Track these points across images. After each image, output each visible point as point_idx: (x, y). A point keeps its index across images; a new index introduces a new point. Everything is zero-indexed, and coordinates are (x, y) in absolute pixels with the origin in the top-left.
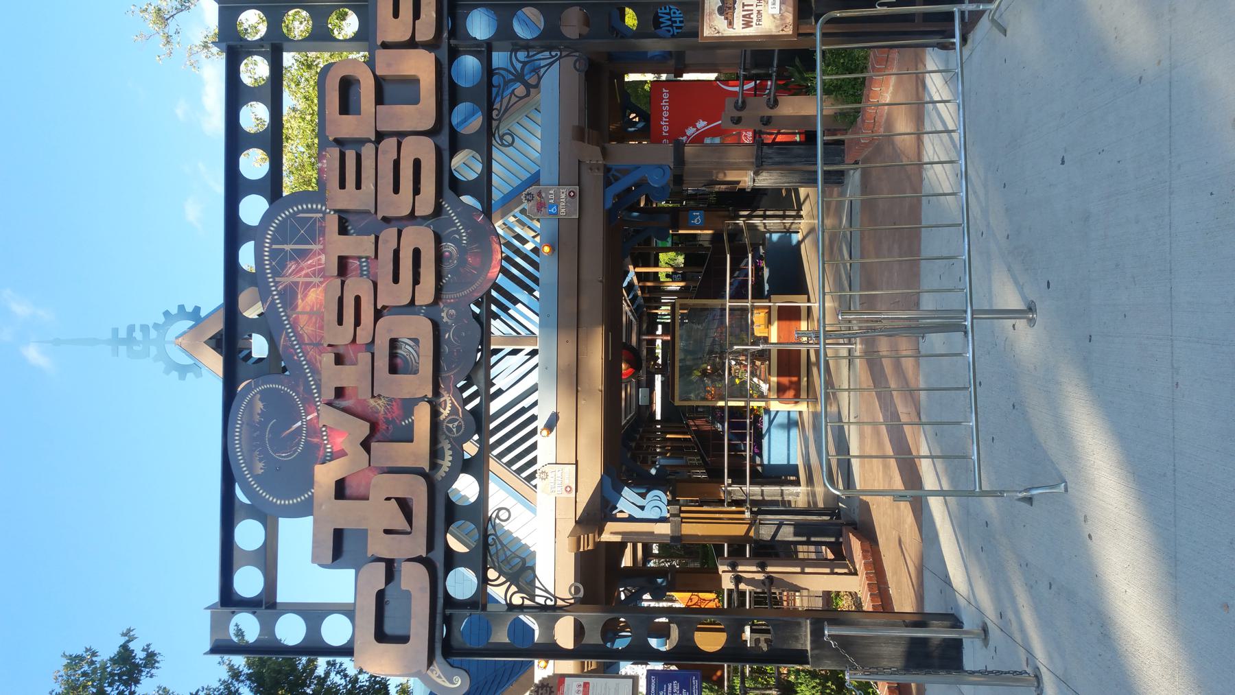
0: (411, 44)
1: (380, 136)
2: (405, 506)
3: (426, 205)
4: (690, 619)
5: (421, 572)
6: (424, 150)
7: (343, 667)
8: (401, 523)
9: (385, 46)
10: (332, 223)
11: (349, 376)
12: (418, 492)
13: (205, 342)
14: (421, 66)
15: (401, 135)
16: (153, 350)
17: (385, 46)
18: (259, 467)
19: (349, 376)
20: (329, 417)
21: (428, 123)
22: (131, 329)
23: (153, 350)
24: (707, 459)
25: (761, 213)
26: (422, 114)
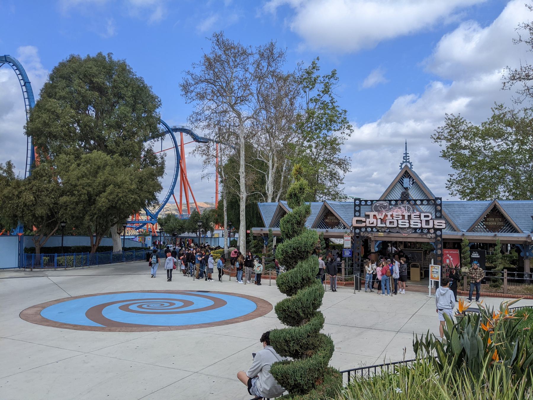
0: (434, 225)
1: (421, 220)
2: (373, 223)
3: (412, 226)
4: (334, 112)
5: (365, 225)
6: (419, 226)
7: (336, 72)
8: (370, 223)
9: (433, 221)
10: (409, 214)
11: (389, 217)
12: (375, 225)
13: (406, 171)
14: (431, 226)
15: (421, 223)
16: (405, 161)
17: (433, 221)
18: (377, 205)
19: (389, 217)
20: (384, 214)
21: (423, 227)
22: (409, 156)
23: (405, 161)
24: (486, 255)
25: (85, 241)
26: (424, 226)
